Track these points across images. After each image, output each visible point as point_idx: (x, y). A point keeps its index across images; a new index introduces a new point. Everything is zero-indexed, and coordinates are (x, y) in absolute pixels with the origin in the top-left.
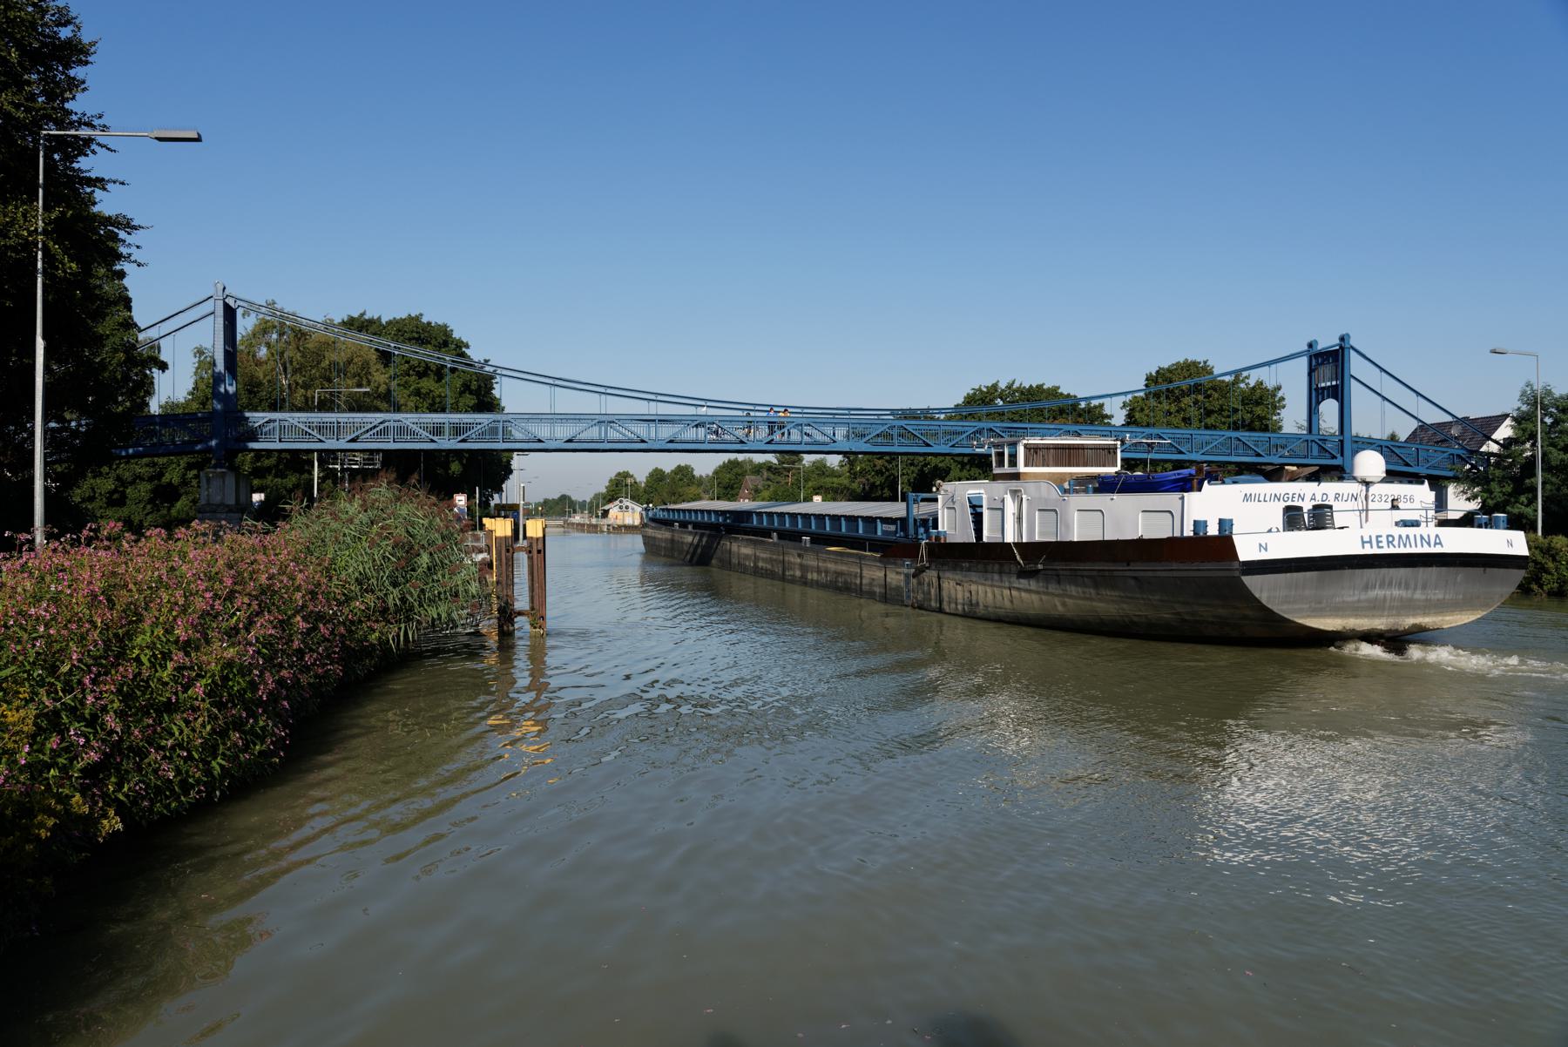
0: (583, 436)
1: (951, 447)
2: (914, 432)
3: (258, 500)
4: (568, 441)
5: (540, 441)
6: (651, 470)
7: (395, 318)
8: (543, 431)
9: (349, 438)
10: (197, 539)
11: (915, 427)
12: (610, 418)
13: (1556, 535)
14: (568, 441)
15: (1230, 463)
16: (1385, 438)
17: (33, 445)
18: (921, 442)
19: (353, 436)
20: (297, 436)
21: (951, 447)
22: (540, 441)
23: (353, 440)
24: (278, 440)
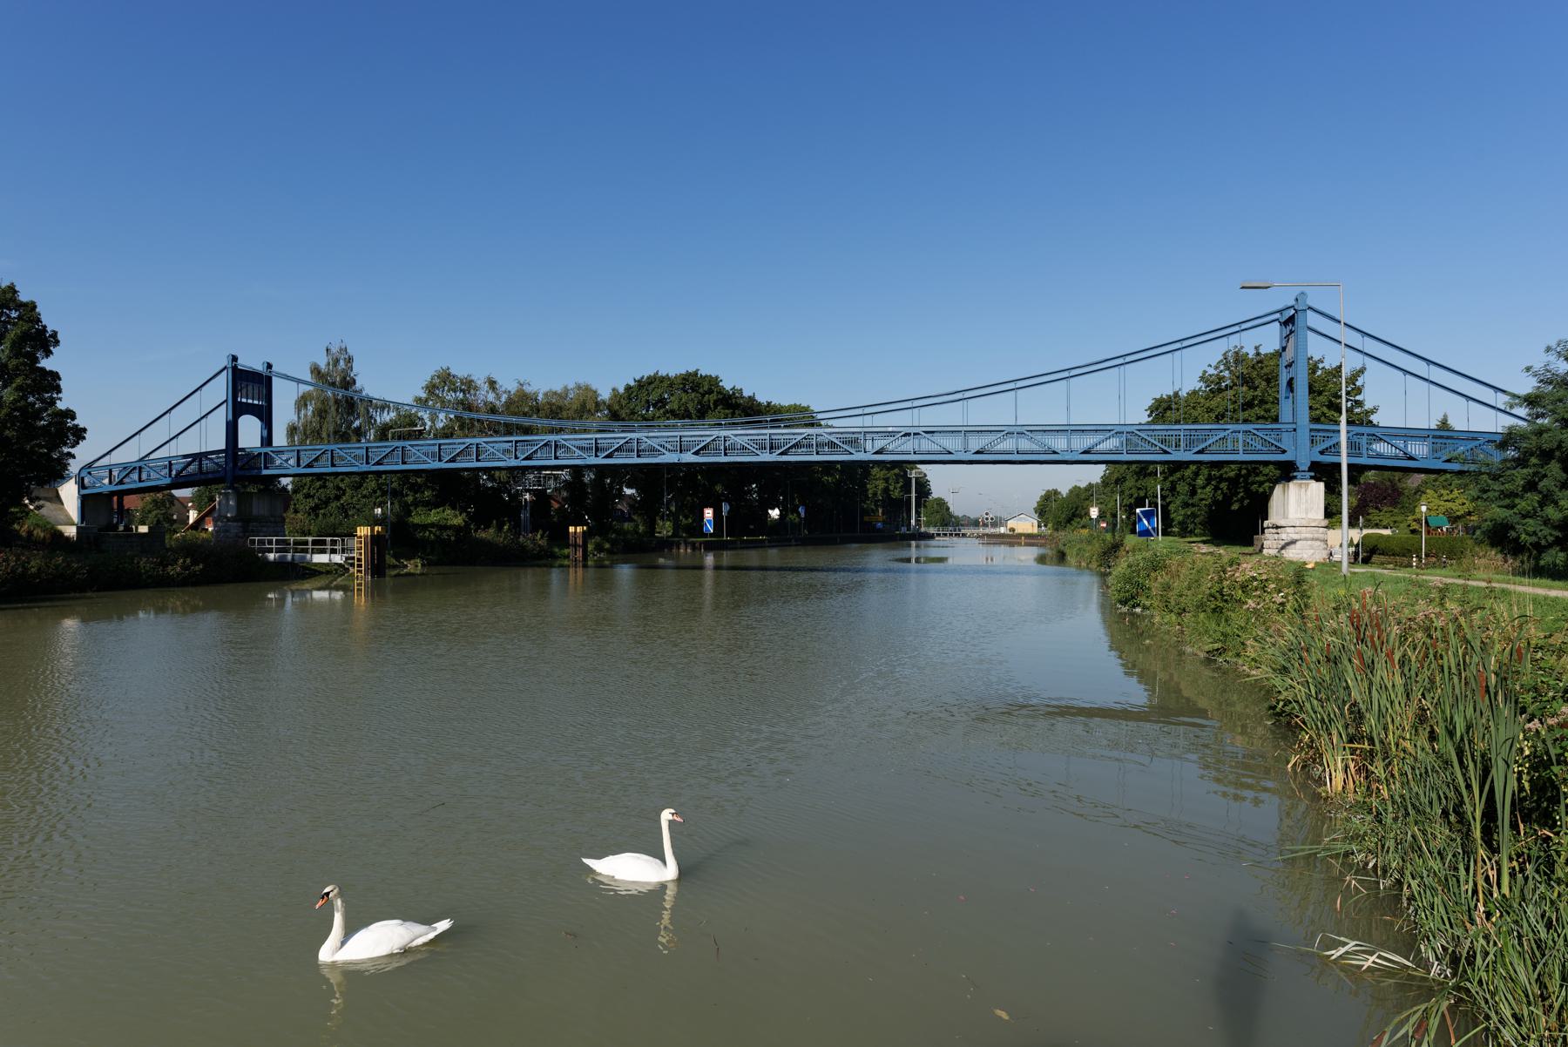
0: (1101, 447)
1: (778, 455)
2: (1149, 439)
3: (1126, 541)
4: (978, 452)
5: (1055, 452)
6: (1071, 487)
7: (769, 403)
8: (1060, 443)
9: (1196, 449)
10: (1203, 703)
11: (666, 439)
12: (1019, 429)
13: (489, 541)
14: (978, 452)
15: (1266, 463)
16: (1433, 426)
17: (838, 462)
18: (1274, 448)
19: (1200, 448)
20: (1221, 448)
21: (778, 455)
22: (1055, 452)
23: (1201, 452)
24: (815, 453)
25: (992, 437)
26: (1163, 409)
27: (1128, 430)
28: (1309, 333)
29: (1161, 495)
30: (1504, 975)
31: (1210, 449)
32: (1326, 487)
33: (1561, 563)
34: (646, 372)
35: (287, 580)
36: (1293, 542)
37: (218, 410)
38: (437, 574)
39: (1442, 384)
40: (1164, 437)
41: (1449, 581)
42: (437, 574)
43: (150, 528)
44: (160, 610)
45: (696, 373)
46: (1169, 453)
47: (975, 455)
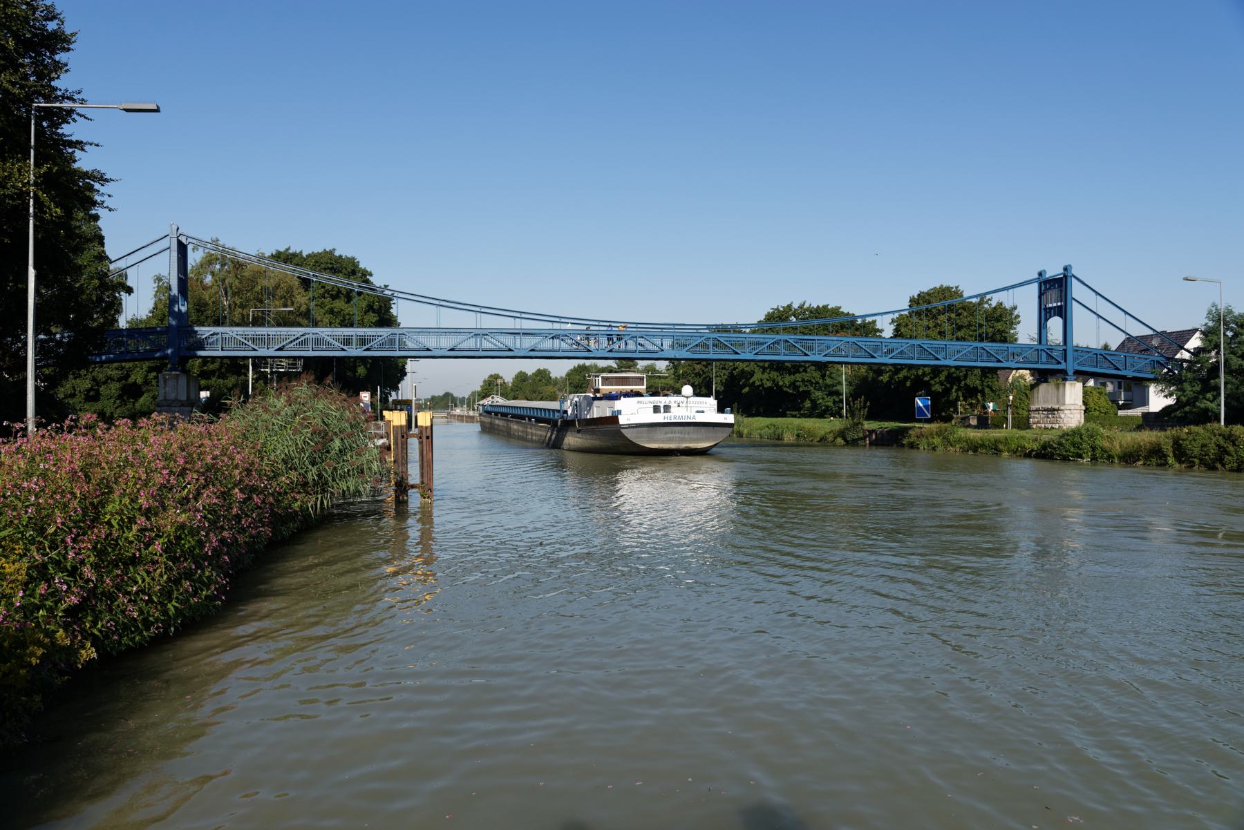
0: (463, 346)
5: (428, 350)
8: (431, 342)
9: (277, 347)
16: (1100, 348)
19: (280, 346)
20: (236, 346)
22: (428, 350)
23: (280, 349)
24: (220, 349)
28: (1073, 301)
29: (843, 403)
31: (288, 346)
32: (202, 391)
33: (1032, 566)
34: (782, 303)
36: (622, 496)
38: (364, 660)
39: (1147, 323)
41: (605, 661)
42: (364, 660)
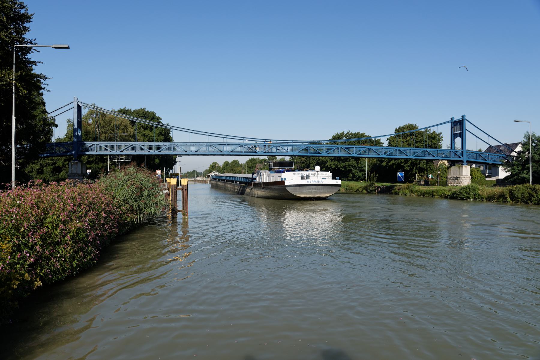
0: (201, 150)
5: (186, 152)
6: (224, 162)
8: (187, 148)
9: (120, 151)
19: (122, 150)
20: (102, 150)
22: (186, 152)
23: (122, 151)
25: (233, 147)
26: (338, 138)
27: (210, 144)
30: (362, 229)
35: (309, 200)
37: (71, 110)
39: (485, 132)
40: (113, 146)
43: (92, 171)
44: (295, 209)
45: (144, 109)
46: (321, 153)
47: (159, 153)
